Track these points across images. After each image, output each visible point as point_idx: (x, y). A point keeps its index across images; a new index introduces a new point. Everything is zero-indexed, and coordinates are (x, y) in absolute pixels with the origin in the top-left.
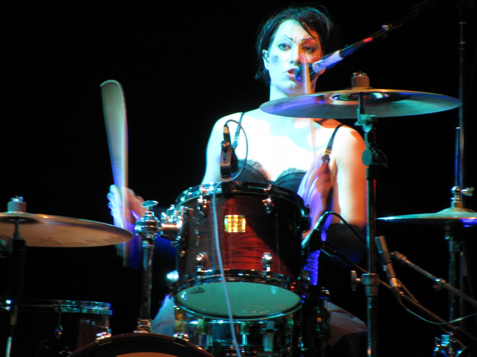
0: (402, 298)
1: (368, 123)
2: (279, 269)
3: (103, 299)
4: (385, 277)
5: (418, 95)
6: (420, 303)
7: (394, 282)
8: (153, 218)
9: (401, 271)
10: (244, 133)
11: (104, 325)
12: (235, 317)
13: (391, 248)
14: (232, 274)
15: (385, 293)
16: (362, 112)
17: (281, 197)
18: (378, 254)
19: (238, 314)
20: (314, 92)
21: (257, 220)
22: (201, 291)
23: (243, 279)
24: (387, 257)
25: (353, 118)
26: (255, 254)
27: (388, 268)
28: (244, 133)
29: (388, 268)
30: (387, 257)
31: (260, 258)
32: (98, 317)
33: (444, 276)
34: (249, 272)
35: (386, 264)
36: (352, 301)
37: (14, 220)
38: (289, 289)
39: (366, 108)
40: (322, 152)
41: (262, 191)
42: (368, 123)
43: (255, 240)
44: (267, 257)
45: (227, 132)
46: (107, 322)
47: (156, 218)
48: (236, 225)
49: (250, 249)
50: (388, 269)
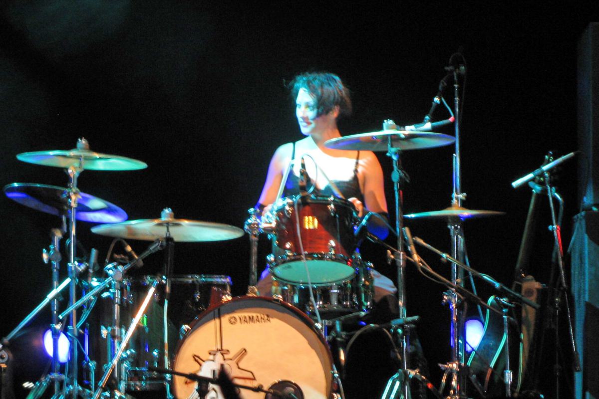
0: (421, 267)
1: (395, 154)
2: (340, 251)
3: (225, 273)
4: (409, 254)
5: (438, 135)
6: (434, 270)
7: (416, 258)
8: (256, 220)
9: (420, 249)
10: (317, 175)
11: (226, 290)
12: (312, 283)
13: (413, 235)
14: (310, 256)
15: (410, 266)
16: (392, 146)
17: (340, 204)
18: (405, 240)
19: (314, 281)
20: (453, 137)
21: (326, 221)
22: (289, 267)
23: (331, 379)
24: (411, 241)
25: (385, 150)
26: (324, 242)
27: (411, 248)
28: (317, 175)
29: (411, 248)
30: (411, 241)
31: (326, 244)
32: (223, 286)
33: (450, 254)
34: (321, 254)
35: (410, 245)
36: (389, 271)
37: (168, 224)
38: (347, 264)
39: (393, 143)
40: (353, 168)
41: (328, 201)
42: (395, 154)
43: (324, 233)
44: (332, 243)
45: (303, 162)
46: (228, 288)
47: (258, 220)
48: (311, 223)
49: (320, 238)
50: (411, 249)
